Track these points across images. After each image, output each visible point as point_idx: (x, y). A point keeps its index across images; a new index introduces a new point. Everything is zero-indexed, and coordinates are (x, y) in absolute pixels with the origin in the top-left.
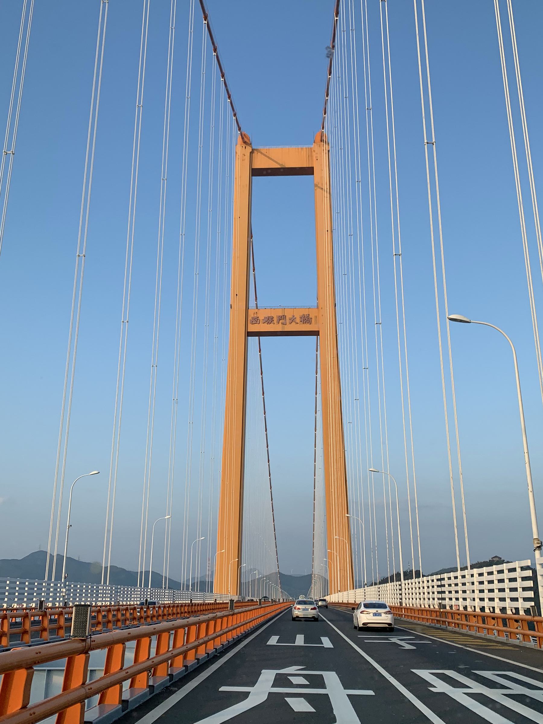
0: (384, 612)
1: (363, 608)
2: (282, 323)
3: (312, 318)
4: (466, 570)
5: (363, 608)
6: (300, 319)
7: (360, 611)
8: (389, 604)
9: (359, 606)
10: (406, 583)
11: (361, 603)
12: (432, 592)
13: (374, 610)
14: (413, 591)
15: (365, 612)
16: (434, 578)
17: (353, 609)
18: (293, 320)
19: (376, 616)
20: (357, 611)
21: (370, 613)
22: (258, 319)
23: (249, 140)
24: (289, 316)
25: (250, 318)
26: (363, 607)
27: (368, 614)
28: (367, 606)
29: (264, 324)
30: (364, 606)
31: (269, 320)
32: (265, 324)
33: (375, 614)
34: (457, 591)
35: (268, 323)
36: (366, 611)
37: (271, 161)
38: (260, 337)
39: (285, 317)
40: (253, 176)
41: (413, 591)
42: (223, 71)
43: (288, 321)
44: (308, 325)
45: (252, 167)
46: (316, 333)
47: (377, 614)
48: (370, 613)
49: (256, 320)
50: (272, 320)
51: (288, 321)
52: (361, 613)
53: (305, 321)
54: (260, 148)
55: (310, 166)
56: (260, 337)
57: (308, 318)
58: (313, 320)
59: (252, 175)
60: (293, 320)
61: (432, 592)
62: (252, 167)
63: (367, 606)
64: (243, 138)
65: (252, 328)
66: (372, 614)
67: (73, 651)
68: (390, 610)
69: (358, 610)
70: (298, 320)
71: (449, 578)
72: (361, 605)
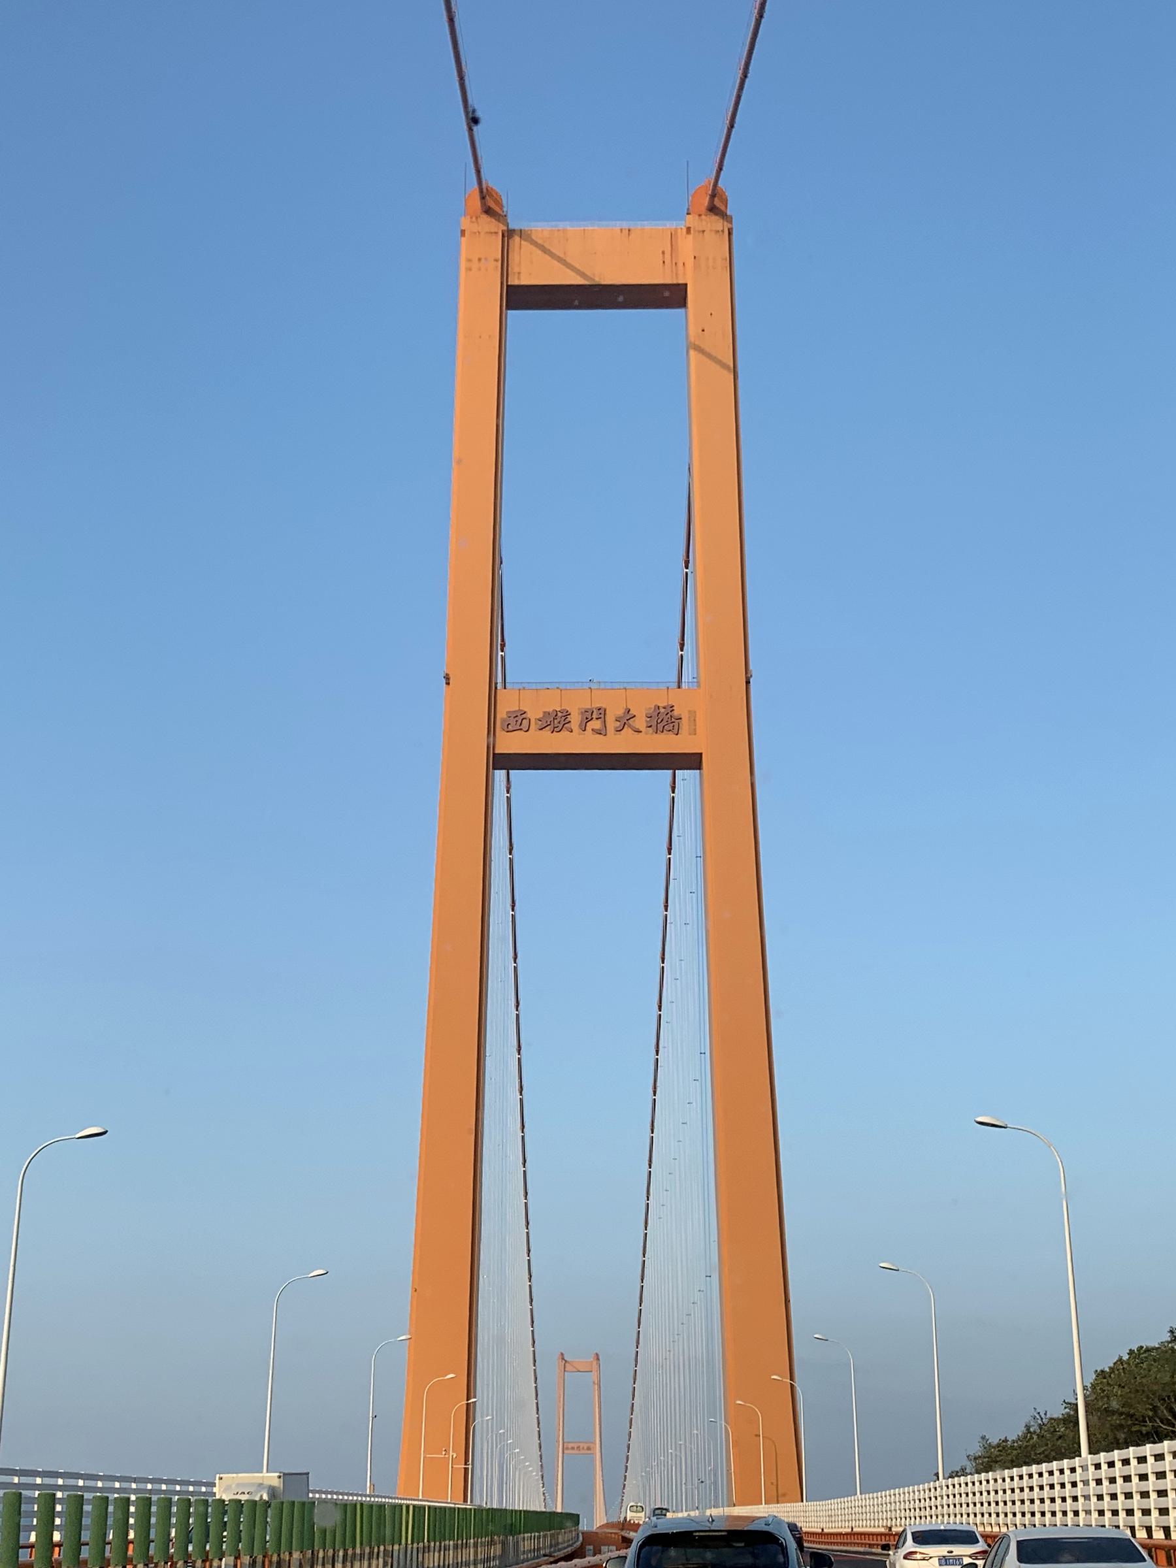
0: (969, 1554)
1: (910, 1546)
2: (592, 730)
3: (682, 717)
4: (1077, 1459)
5: (910, 1546)
6: (648, 719)
7: (902, 1552)
8: (981, 1529)
9: (902, 1541)
10: (990, 1479)
11: (904, 1530)
12: (1098, 1496)
13: (942, 1550)
14: (1133, 1471)
15: (918, 1556)
16: (1075, 1463)
17: (886, 1547)
18: (625, 721)
19: (946, 1564)
20: (894, 1554)
21: (931, 1558)
22: (524, 716)
23: (501, 207)
24: (614, 711)
25: (501, 714)
26: (911, 1541)
27: (924, 1559)
28: (924, 1538)
29: (541, 731)
30: (913, 1539)
31: (557, 721)
32: (546, 732)
33: (943, 1561)
34: (1162, 1491)
35: (554, 728)
36: (920, 1553)
37: (579, 268)
38: (510, 771)
39: (603, 713)
40: (509, 309)
41: (1133, 1471)
42: (454, 8)
43: (612, 724)
44: (671, 736)
45: (507, 282)
46: (693, 761)
47: (951, 1561)
48: (931, 1558)
49: (519, 721)
50: (566, 721)
51: (612, 724)
52: (905, 1558)
53: (660, 726)
54: (540, 229)
55: (681, 282)
56: (510, 771)
57: (669, 716)
58: (685, 725)
59: (509, 307)
60: (625, 721)
61: (1098, 1496)
62: (507, 282)
63: (924, 1538)
64: (483, 198)
65: (510, 744)
66: (935, 1561)
67: (775, 1514)
68: (987, 1547)
69: (899, 1550)
70: (640, 722)
71: (1142, 1460)
72: (906, 1535)
